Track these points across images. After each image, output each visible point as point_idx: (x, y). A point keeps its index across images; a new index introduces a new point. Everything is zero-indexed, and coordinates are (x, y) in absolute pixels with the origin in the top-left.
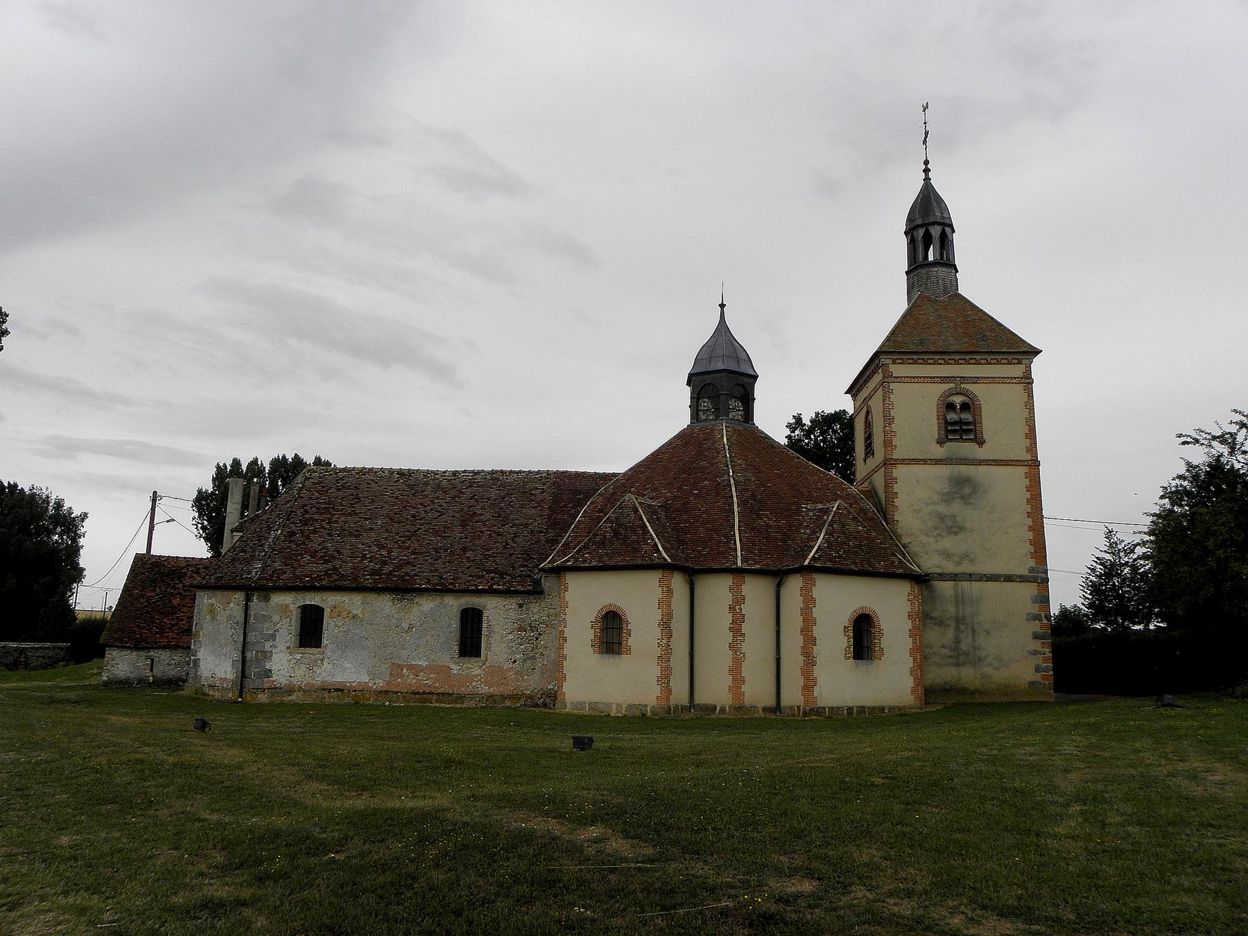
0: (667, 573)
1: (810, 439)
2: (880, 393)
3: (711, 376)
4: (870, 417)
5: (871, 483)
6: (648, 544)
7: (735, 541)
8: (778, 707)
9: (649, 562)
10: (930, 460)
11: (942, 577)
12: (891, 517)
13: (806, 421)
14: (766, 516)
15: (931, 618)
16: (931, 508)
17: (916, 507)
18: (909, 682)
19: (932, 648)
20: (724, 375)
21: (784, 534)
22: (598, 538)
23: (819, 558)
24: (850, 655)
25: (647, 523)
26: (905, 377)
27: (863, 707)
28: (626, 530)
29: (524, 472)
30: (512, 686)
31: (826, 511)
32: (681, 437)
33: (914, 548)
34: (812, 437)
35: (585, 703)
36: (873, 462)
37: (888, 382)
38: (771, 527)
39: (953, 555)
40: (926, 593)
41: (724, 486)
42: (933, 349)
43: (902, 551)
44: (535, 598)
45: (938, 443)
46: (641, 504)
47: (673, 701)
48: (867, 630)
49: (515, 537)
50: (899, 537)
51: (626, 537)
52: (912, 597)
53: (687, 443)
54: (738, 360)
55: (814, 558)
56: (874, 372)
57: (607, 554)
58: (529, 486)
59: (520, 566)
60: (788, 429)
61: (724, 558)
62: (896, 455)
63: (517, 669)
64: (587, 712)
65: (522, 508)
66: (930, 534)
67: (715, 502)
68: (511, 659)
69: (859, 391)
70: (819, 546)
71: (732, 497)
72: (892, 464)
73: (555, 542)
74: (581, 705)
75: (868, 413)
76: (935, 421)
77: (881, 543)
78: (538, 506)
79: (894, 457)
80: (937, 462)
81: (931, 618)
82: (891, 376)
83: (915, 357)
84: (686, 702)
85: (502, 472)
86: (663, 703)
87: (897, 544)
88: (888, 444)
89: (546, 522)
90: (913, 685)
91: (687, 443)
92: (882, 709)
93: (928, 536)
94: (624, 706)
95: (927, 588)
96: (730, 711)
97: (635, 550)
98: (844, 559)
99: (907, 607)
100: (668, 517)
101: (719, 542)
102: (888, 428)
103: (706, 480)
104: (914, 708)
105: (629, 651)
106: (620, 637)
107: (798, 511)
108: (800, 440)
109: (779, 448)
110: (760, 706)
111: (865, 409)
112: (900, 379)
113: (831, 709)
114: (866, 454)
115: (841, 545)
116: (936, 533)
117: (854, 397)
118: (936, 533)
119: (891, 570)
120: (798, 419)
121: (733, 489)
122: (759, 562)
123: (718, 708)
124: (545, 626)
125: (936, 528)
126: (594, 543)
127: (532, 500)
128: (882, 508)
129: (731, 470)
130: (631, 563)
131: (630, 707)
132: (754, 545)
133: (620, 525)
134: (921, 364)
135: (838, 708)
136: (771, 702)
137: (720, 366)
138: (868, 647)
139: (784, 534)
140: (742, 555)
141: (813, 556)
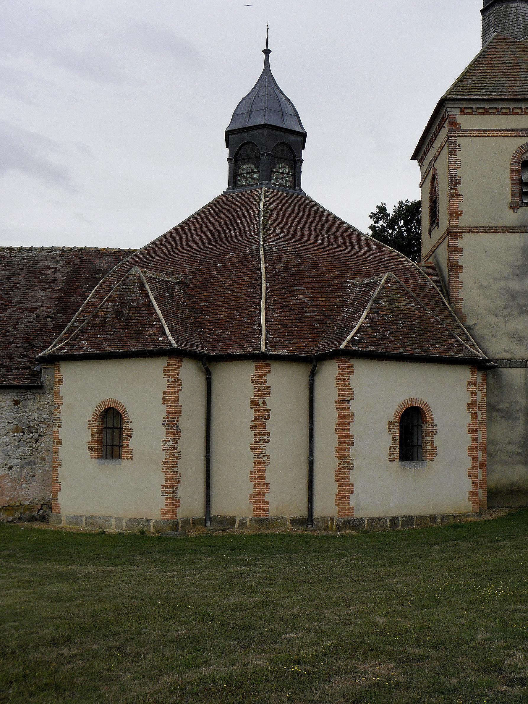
0: (173, 360)
1: (394, 229)
2: (446, 150)
3: (251, 133)
4: (436, 182)
5: (435, 258)
6: (153, 326)
7: (260, 321)
8: (310, 518)
9: (152, 348)
10: (501, 227)
11: (511, 363)
12: (454, 295)
13: (390, 211)
14: (302, 292)
15: (498, 410)
16: (500, 284)
17: (484, 283)
18: (468, 486)
19: (497, 444)
20: (265, 131)
21: (323, 313)
22: (98, 321)
23: (359, 341)
24: (395, 456)
25: (154, 302)
26: (474, 130)
27: (411, 517)
28: (129, 310)
29: (36, 249)
30: (8, 496)
31: (372, 286)
32: (215, 205)
33: (480, 330)
34: (396, 227)
35: (81, 517)
36: (438, 233)
37: (455, 137)
38: (306, 305)
39: (524, 338)
40: (492, 381)
41: (252, 257)
42: (508, 96)
43: (465, 334)
44: (33, 394)
45: (511, 207)
46: (149, 279)
47: (181, 514)
48: (418, 426)
49: (17, 323)
50: (462, 318)
51: (129, 318)
52: (472, 386)
53: (219, 212)
54: (282, 114)
55: (352, 340)
56: (440, 127)
57: (106, 340)
58: (40, 265)
59: (20, 357)
60: (372, 220)
61: (246, 342)
62: (463, 222)
63: (14, 476)
64: (83, 527)
65: (29, 289)
66: (499, 314)
67: (241, 276)
68: (6, 465)
69: (425, 154)
70: (360, 326)
71: (260, 269)
72: (456, 233)
73: (61, 328)
74: (76, 519)
75: (434, 178)
76: (508, 181)
77: (438, 323)
78: (49, 288)
79: (461, 224)
80: (509, 230)
81: (498, 410)
82: (459, 129)
83: (487, 106)
84: (200, 513)
85: (10, 249)
86: (168, 517)
87: (460, 326)
88: (453, 209)
89: (56, 306)
90: (471, 489)
91: (219, 212)
92: (433, 518)
93: (496, 316)
94: (125, 521)
95: (494, 376)
96: (250, 525)
97: (139, 334)
98: (391, 342)
99: (467, 398)
100: (187, 296)
101: (242, 323)
102: (453, 191)
103: (233, 250)
104: (468, 516)
105: (130, 456)
106: (120, 438)
107: (342, 287)
108: (384, 231)
109: (328, 216)
110: (288, 517)
111: (431, 174)
112: (468, 133)
113: (371, 521)
114: (432, 225)
115: (387, 325)
116: (505, 312)
117: (421, 163)
118: (505, 312)
119: (447, 355)
120: (382, 209)
121: (262, 260)
122: (289, 347)
123: (238, 521)
124: (45, 426)
125: (506, 307)
126: (93, 327)
127: (41, 281)
128: (445, 285)
129: (261, 239)
130: (133, 349)
131: (132, 521)
132: (284, 326)
133: (123, 304)
134: (494, 114)
135: (379, 519)
136: (301, 512)
137: (260, 120)
138: (418, 446)
139: (323, 313)
140: (267, 338)
141: (352, 338)
